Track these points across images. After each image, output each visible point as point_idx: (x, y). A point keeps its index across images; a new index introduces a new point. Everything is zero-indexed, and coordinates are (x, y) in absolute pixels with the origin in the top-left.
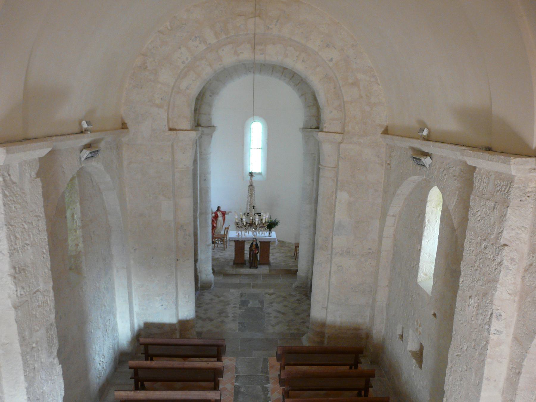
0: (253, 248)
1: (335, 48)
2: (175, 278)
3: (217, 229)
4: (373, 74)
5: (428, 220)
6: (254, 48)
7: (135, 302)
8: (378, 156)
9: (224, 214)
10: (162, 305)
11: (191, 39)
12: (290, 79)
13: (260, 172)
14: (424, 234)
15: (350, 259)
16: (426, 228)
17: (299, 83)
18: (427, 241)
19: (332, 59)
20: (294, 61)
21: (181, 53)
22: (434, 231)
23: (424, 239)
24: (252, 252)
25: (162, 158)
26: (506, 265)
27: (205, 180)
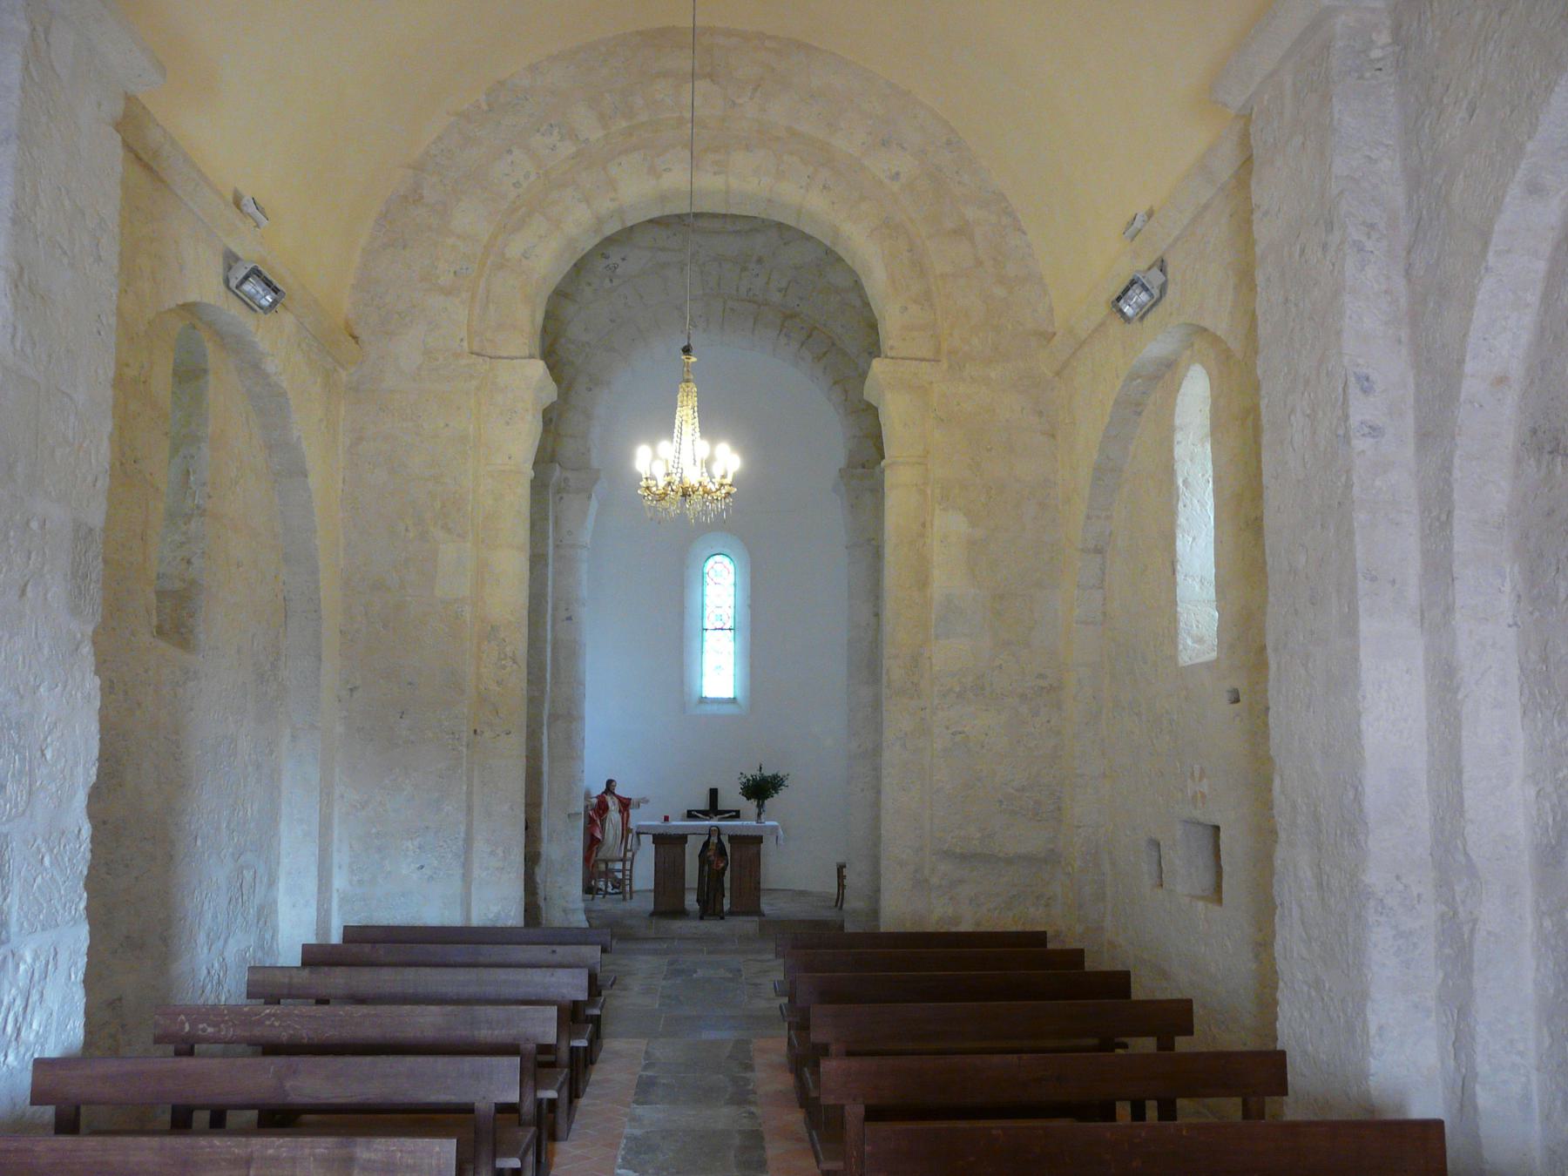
0: (709, 854)
1: (903, 148)
2: (465, 778)
3: (604, 848)
4: (1006, 208)
5: (1185, 482)
6: (694, 159)
7: (340, 856)
8: (1041, 414)
9: (625, 805)
10: (422, 867)
11: (538, 131)
12: (802, 344)
13: (732, 697)
14: (1179, 522)
15: (987, 710)
16: (1181, 505)
17: (825, 354)
18: (1190, 539)
19: (898, 174)
20: (801, 187)
21: (512, 162)
22: (1206, 511)
23: (1181, 536)
24: (707, 868)
25: (447, 425)
26: (1356, 238)
27: (569, 618)
